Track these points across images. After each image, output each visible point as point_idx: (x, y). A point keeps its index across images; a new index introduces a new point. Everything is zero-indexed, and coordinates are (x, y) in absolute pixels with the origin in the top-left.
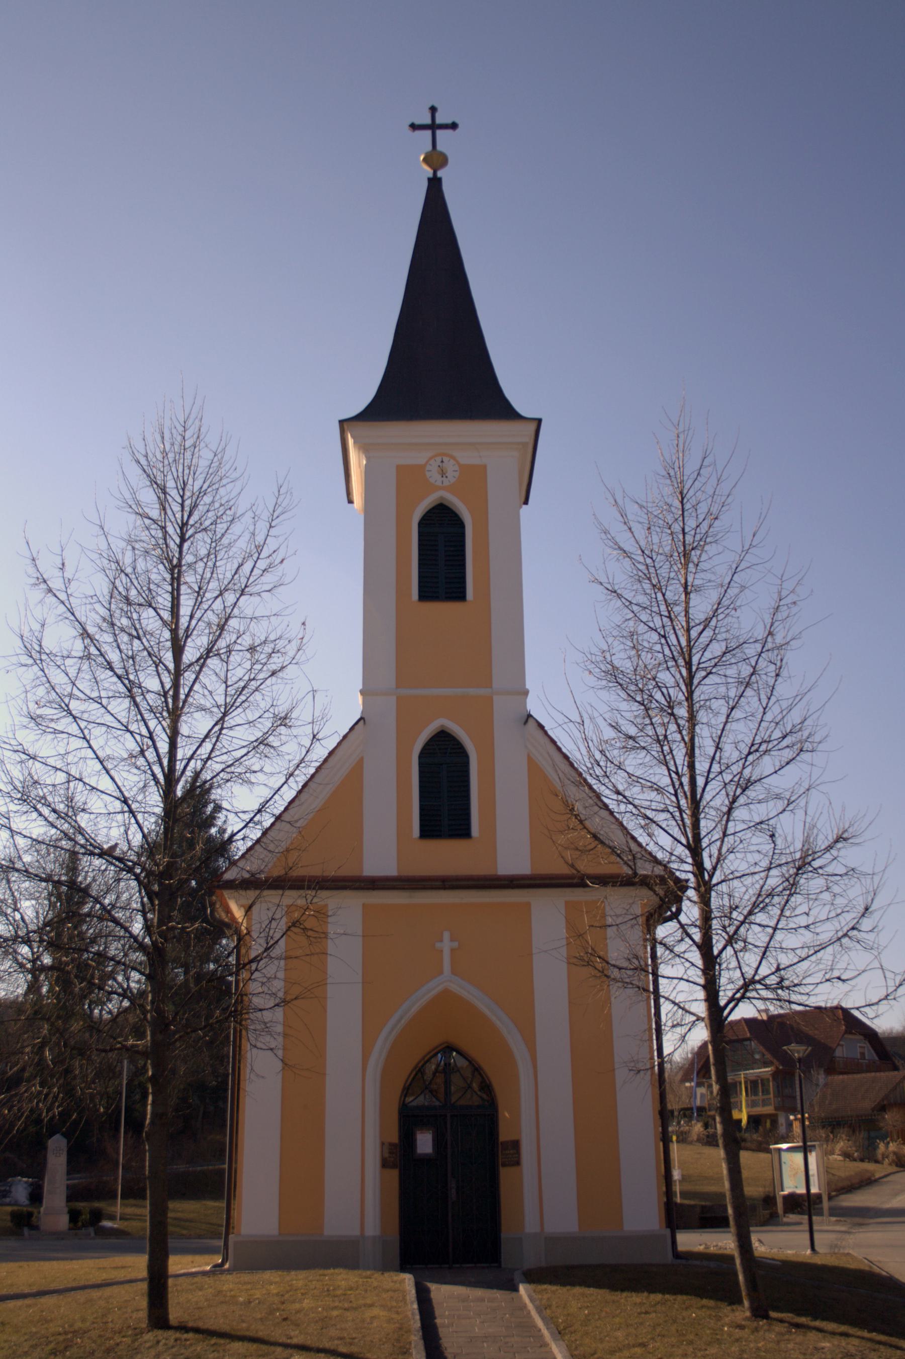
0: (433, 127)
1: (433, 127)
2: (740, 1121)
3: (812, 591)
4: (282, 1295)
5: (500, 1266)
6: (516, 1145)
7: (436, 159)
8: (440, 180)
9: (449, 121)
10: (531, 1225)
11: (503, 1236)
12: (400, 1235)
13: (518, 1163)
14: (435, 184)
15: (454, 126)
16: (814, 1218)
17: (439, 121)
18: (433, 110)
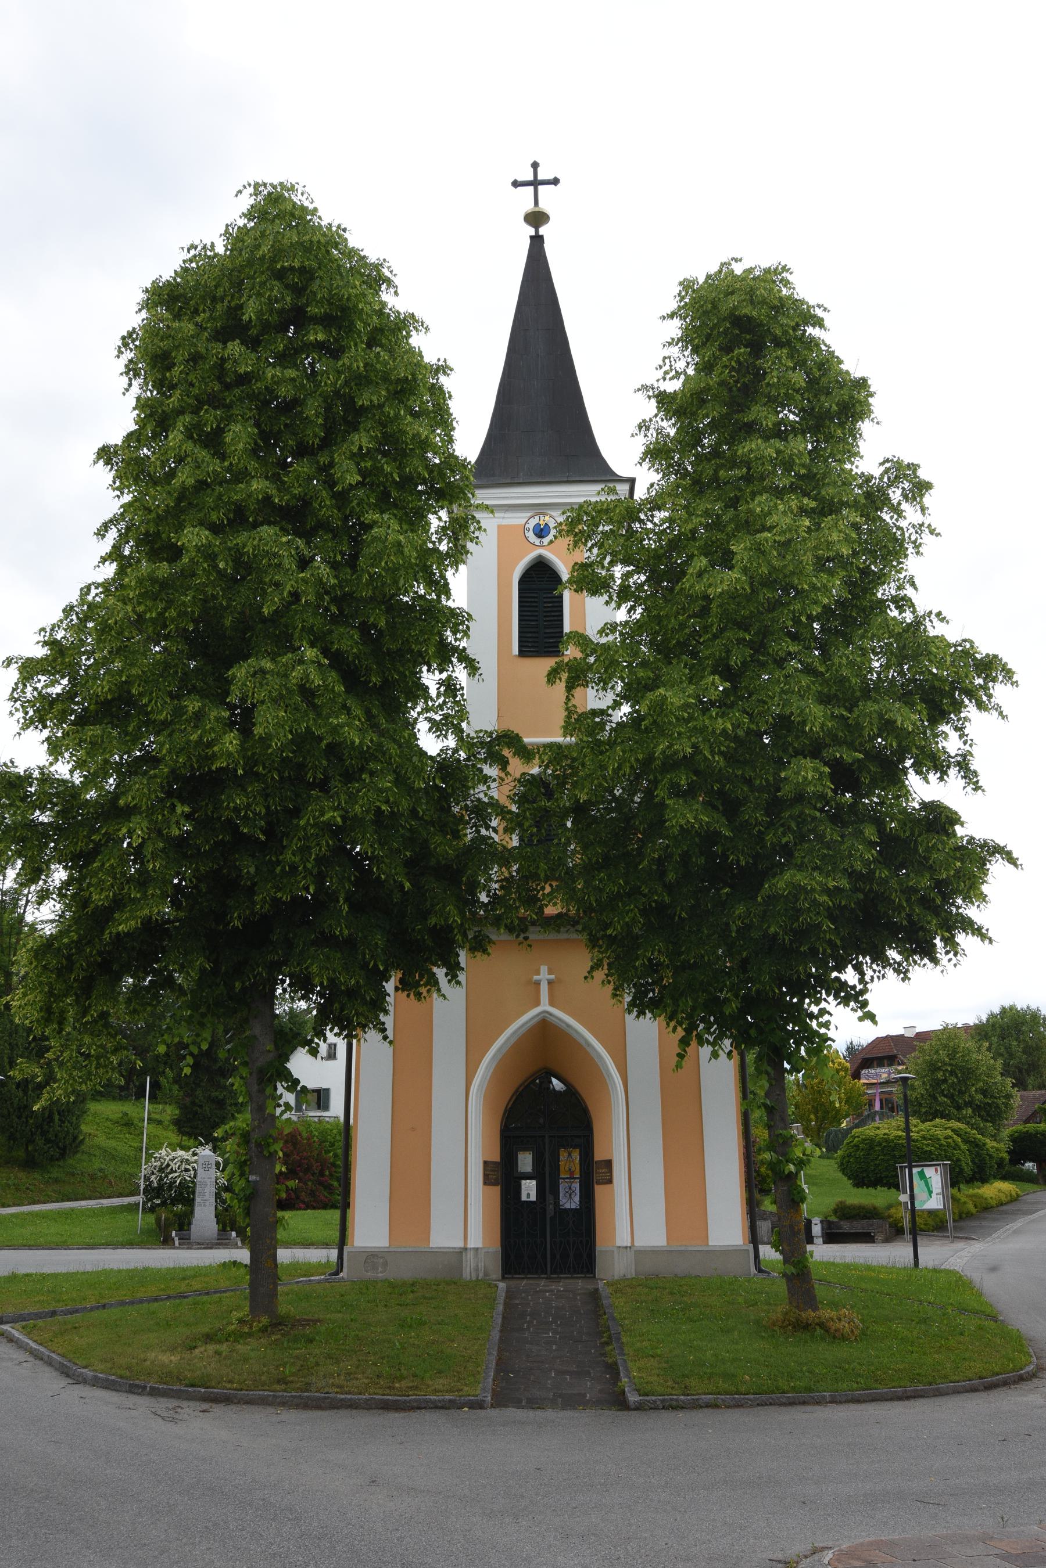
0: (535, 183)
1: (535, 183)
2: (538, 974)
3: (741, 260)
4: (342, 1296)
5: (594, 1277)
6: (608, 1164)
7: (536, 218)
8: (542, 237)
9: (551, 177)
10: (622, 1238)
11: (598, 1248)
12: (502, 1246)
13: (610, 1181)
14: (537, 241)
15: (555, 181)
16: (919, 1239)
17: (540, 177)
18: (535, 165)
